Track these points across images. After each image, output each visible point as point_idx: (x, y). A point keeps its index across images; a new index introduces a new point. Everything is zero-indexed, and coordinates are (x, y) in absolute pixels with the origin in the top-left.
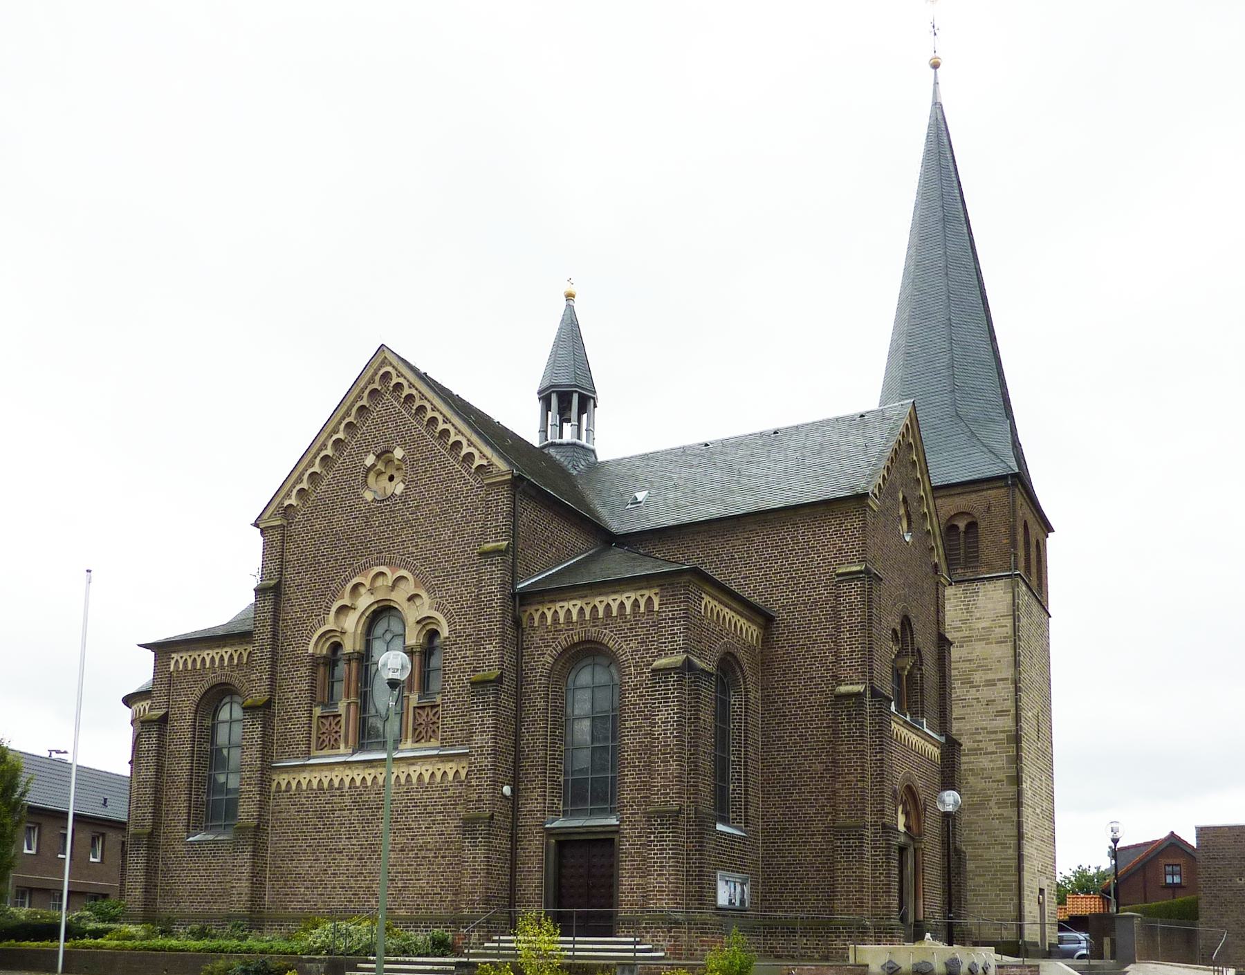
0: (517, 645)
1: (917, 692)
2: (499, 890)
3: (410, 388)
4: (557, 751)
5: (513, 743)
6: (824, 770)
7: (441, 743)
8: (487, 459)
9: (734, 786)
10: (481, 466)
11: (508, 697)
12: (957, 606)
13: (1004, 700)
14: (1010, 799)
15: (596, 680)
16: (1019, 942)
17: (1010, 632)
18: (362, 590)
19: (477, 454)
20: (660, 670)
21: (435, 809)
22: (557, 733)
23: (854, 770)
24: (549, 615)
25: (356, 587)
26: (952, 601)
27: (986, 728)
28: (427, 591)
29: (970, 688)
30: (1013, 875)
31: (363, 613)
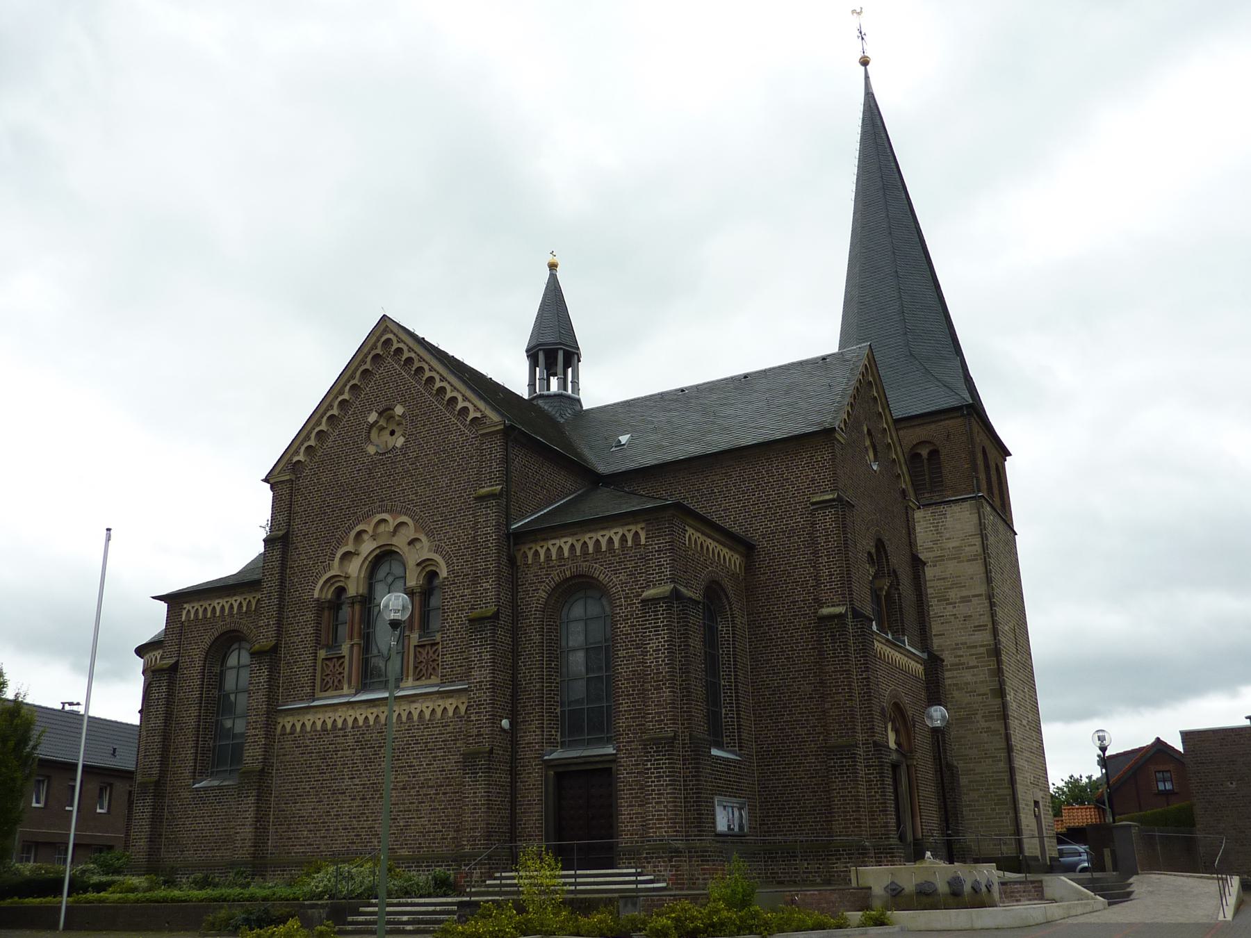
7: (441, 680)
8: (481, 412)
9: (726, 710)
10: (475, 419)
12: (927, 528)
13: (980, 615)
14: (995, 712)
17: (980, 550)
18: (365, 537)
20: (649, 600)
21: (435, 746)
22: (553, 666)
24: (542, 552)
25: (360, 534)
27: (966, 643)
28: (427, 535)
30: (1006, 788)
31: (366, 558)
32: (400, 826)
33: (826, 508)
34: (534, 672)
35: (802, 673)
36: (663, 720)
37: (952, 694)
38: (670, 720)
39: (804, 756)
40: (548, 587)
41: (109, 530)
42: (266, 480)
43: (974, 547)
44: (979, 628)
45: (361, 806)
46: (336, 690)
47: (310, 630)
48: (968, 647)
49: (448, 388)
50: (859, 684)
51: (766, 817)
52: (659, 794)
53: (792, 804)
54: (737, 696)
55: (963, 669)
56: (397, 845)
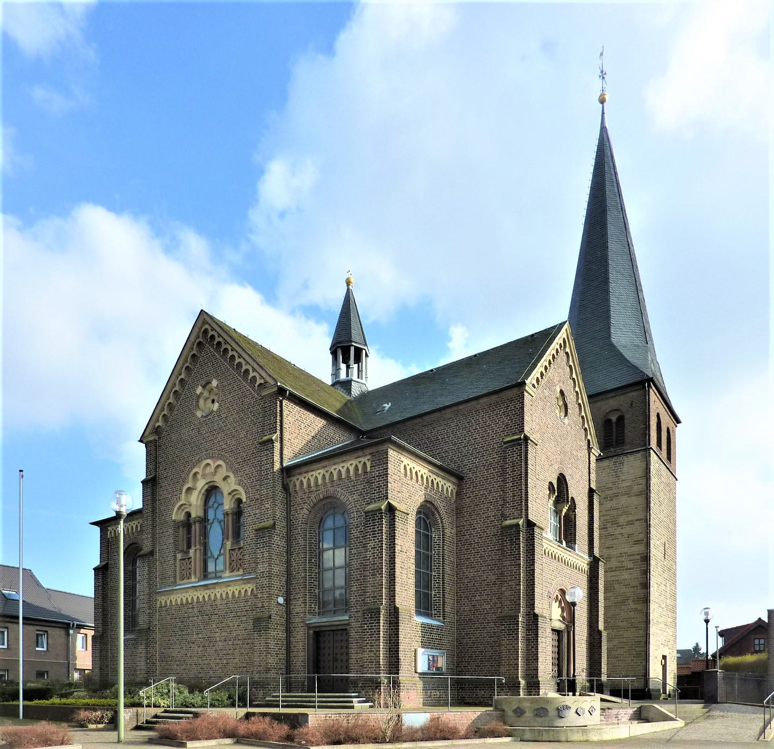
0: (287, 504)
1: (572, 527)
2: (278, 664)
3: (212, 330)
4: (313, 573)
6: (496, 579)
7: (244, 572)
8: (264, 379)
9: (435, 592)
10: (261, 384)
11: (280, 538)
12: (609, 473)
13: (639, 533)
14: (642, 598)
15: (336, 524)
17: (645, 488)
18: (199, 476)
19: (258, 376)
20: (370, 512)
21: (242, 614)
22: (313, 561)
24: (305, 481)
25: (195, 474)
26: (606, 470)
27: (627, 553)
28: (234, 473)
29: (617, 527)
30: (642, 647)
31: (200, 492)
32: (224, 663)
33: (514, 445)
34: (301, 565)
35: (490, 567)
36: (376, 597)
37: (614, 586)
38: (367, 592)
39: (487, 623)
40: (309, 506)
41: (21, 471)
42: (141, 441)
43: (641, 486)
44: (637, 542)
45: (203, 651)
46: (188, 579)
47: (171, 541)
49: (243, 363)
51: (460, 662)
52: (371, 646)
53: (478, 654)
54: (443, 583)
56: (222, 675)
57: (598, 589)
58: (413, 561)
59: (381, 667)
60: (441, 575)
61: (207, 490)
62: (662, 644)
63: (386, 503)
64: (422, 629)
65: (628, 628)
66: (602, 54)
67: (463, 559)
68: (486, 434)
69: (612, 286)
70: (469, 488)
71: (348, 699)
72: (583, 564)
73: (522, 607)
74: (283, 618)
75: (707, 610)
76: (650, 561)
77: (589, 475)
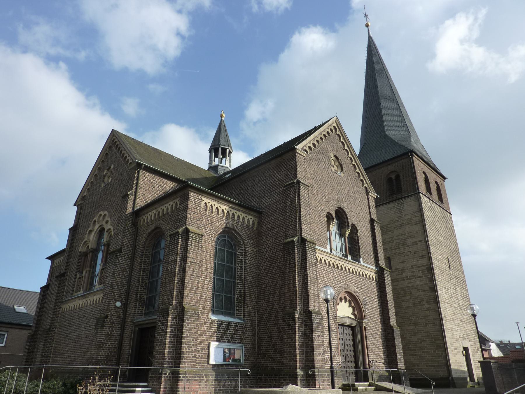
1: (356, 245)
5: (127, 281)
9: (237, 296)
13: (422, 250)
16: (449, 378)
23: (292, 281)
25: (95, 221)
27: (416, 265)
30: (440, 340)
31: (96, 232)
33: (291, 187)
37: (411, 291)
42: (75, 205)
44: (422, 257)
48: (417, 267)
50: (303, 278)
55: (415, 278)
57: (386, 292)
58: (211, 271)
59: (166, 359)
60: (243, 282)
61: (100, 231)
62: (460, 337)
63: (184, 227)
64: (218, 326)
65: (427, 324)
66: (364, 8)
67: (262, 270)
68: (275, 182)
69: (383, 106)
70: (265, 219)
71: (132, 389)
72: (369, 273)
73: (299, 305)
74: (120, 318)
75: (472, 306)
76: (433, 270)
77: (370, 210)
